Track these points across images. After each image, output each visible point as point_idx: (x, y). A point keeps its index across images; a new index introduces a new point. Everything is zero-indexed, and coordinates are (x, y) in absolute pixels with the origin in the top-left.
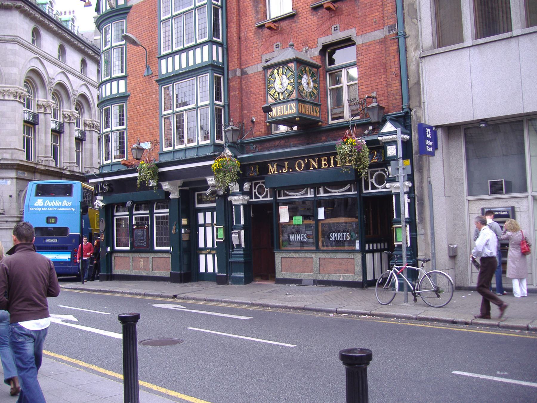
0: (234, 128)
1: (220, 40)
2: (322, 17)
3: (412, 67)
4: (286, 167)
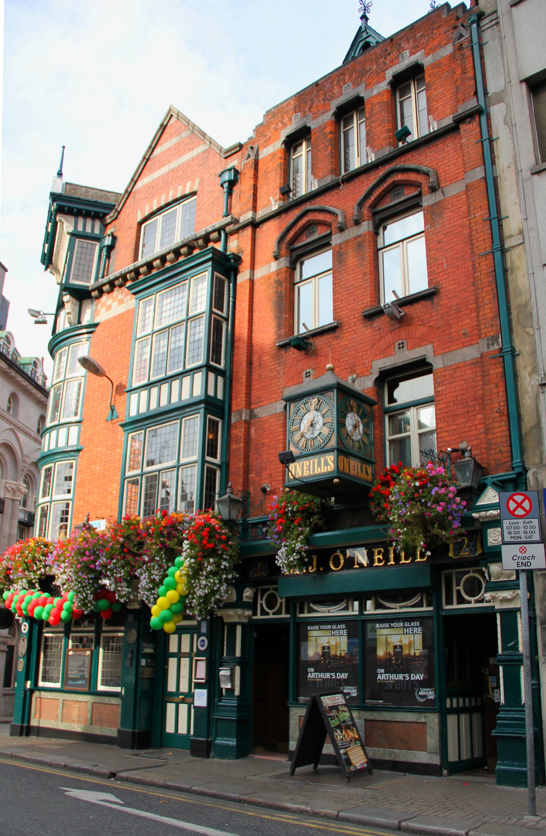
0: (233, 496)
1: (222, 366)
2: (380, 329)
3: (527, 402)
4: (315, 563)
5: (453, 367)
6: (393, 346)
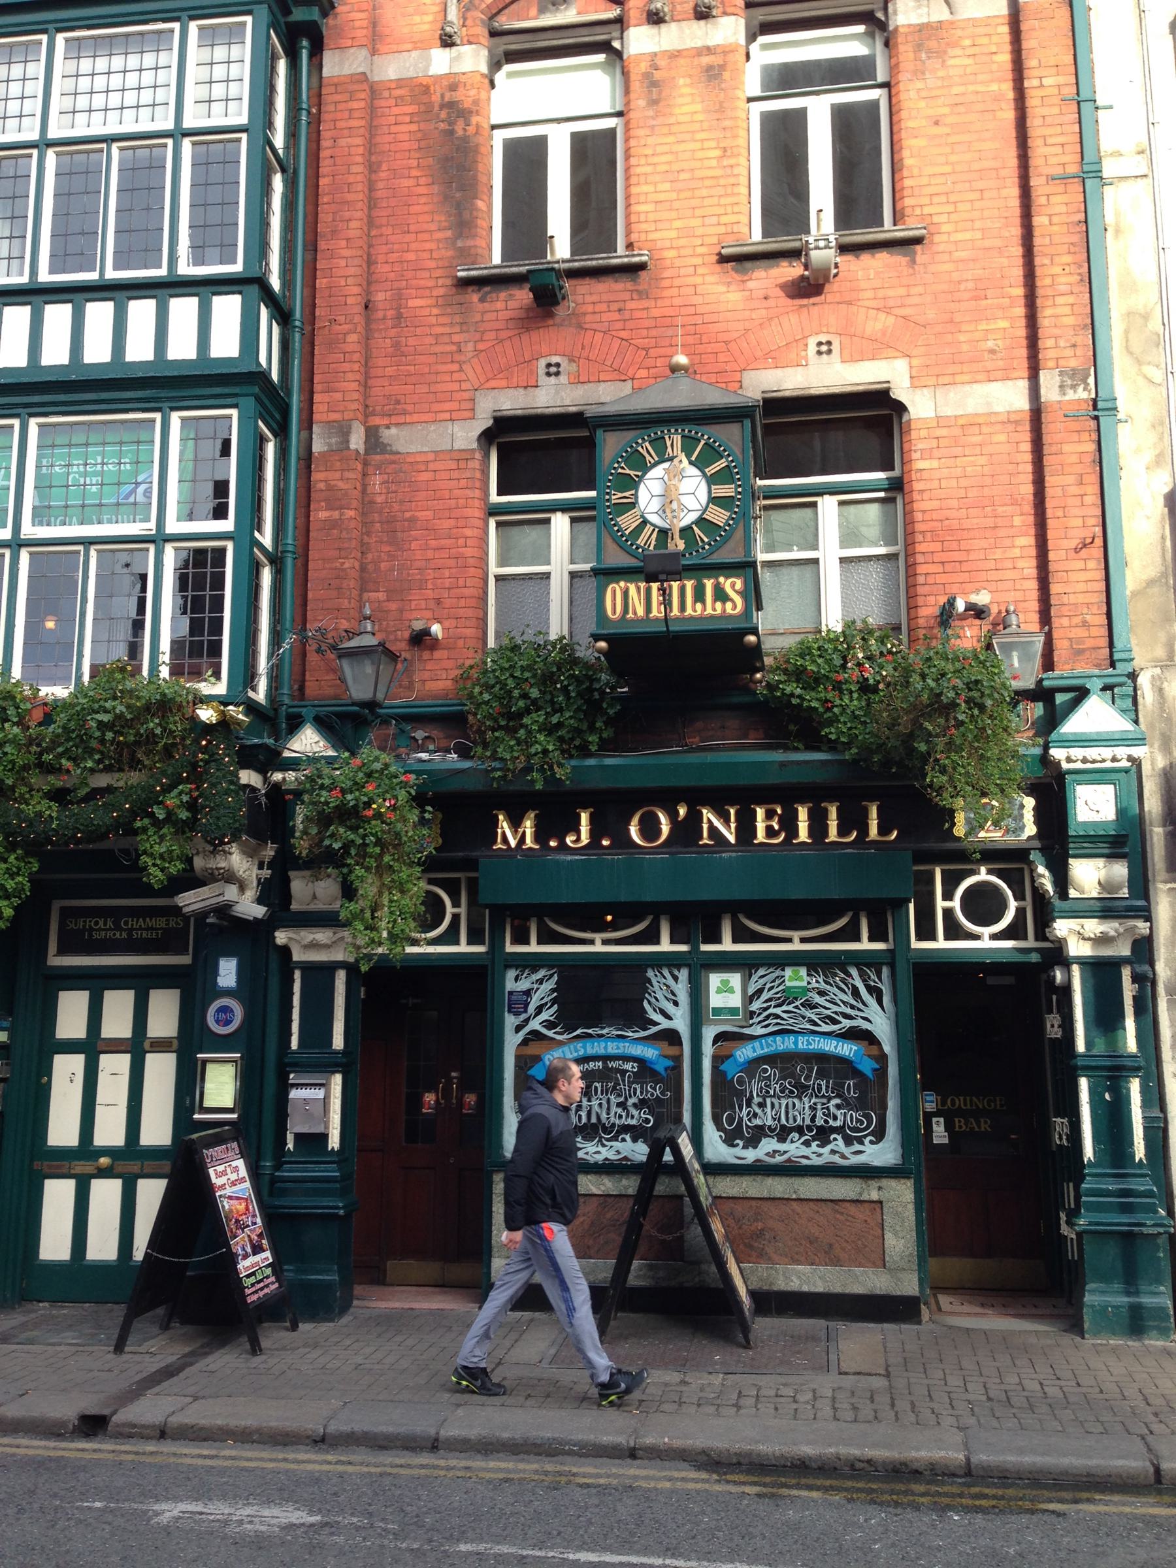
5: (961, 422)
6: (801, 345)
